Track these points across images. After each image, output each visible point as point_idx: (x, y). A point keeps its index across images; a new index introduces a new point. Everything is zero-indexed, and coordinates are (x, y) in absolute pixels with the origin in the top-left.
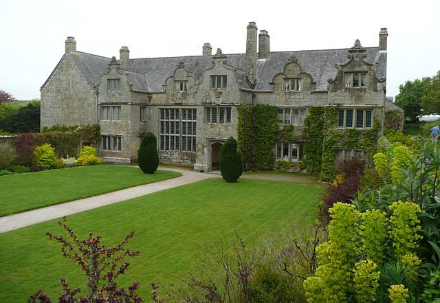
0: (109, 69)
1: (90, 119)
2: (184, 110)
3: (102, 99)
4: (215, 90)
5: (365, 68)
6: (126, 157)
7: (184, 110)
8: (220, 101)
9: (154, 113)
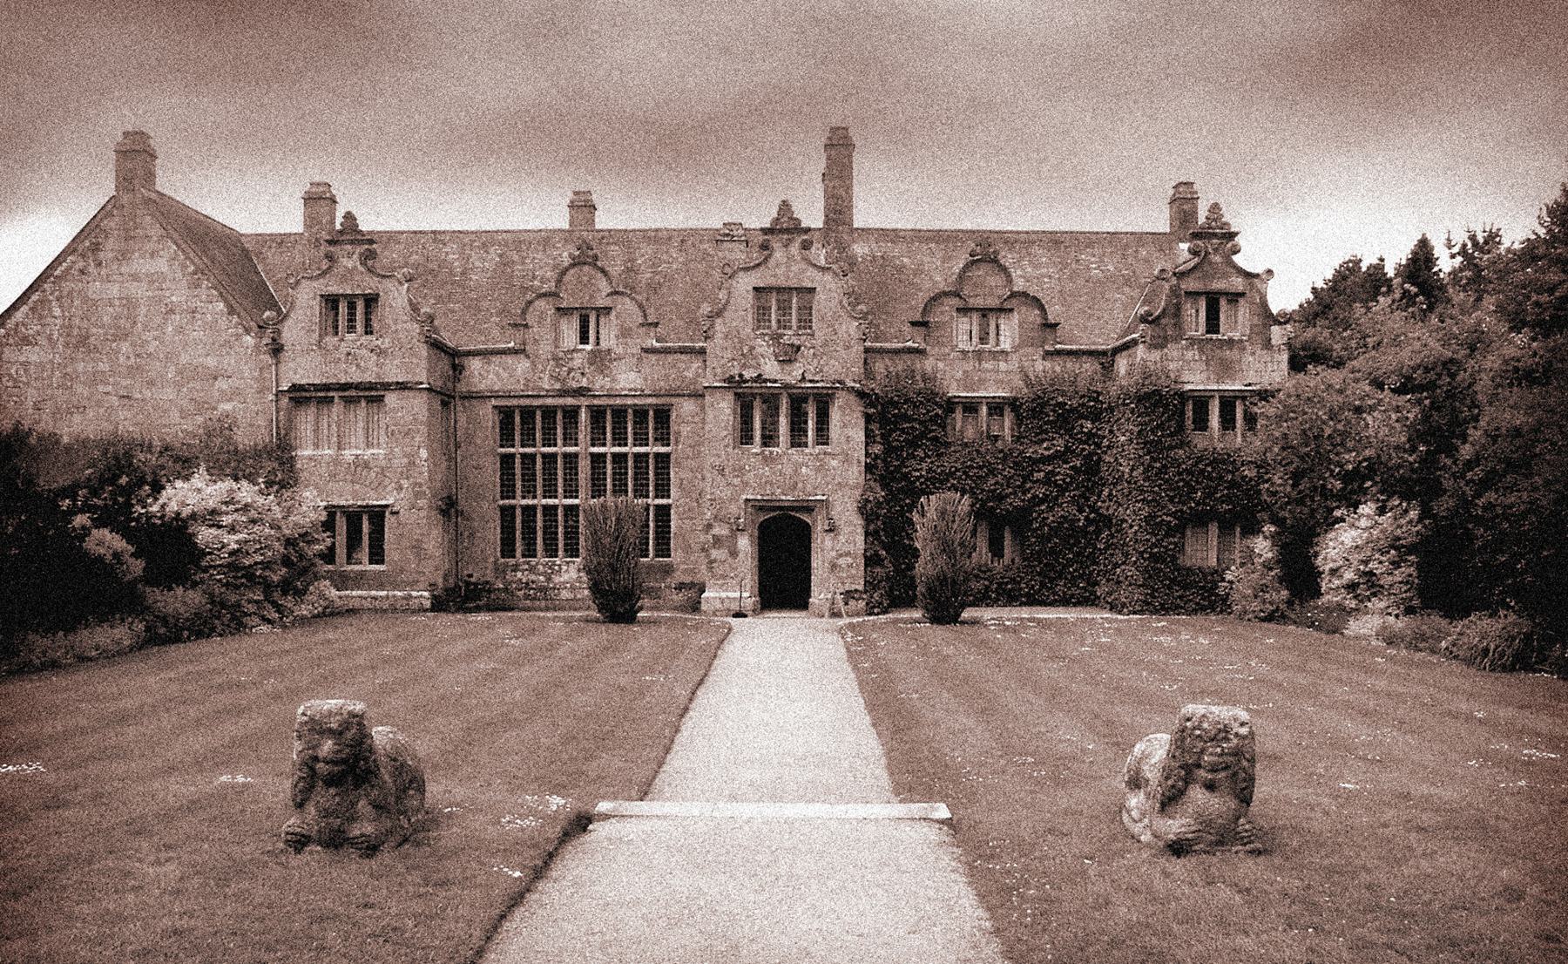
4: (776, 338)
5: (1238, 283)
6: (413, 584)
7: (597, 414)
8: (793, 374)
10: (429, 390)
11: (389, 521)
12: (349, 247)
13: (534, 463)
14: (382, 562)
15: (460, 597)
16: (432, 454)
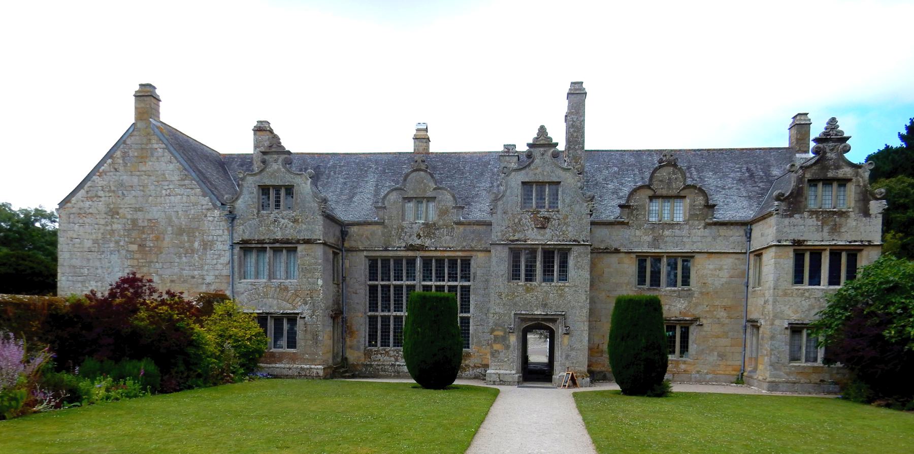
0: (264, 162)
1: (209, 279)
2: (427, 262)
3: (243, 232)
6: (313, 361)
7: (427, 262)
9: (358, 267)
10: (325, 244)
11: (300, 322)
12: (276, 156)
13: (389, 291)
14: (295, 347)
15: (340, 369)
16: (325, 281)
